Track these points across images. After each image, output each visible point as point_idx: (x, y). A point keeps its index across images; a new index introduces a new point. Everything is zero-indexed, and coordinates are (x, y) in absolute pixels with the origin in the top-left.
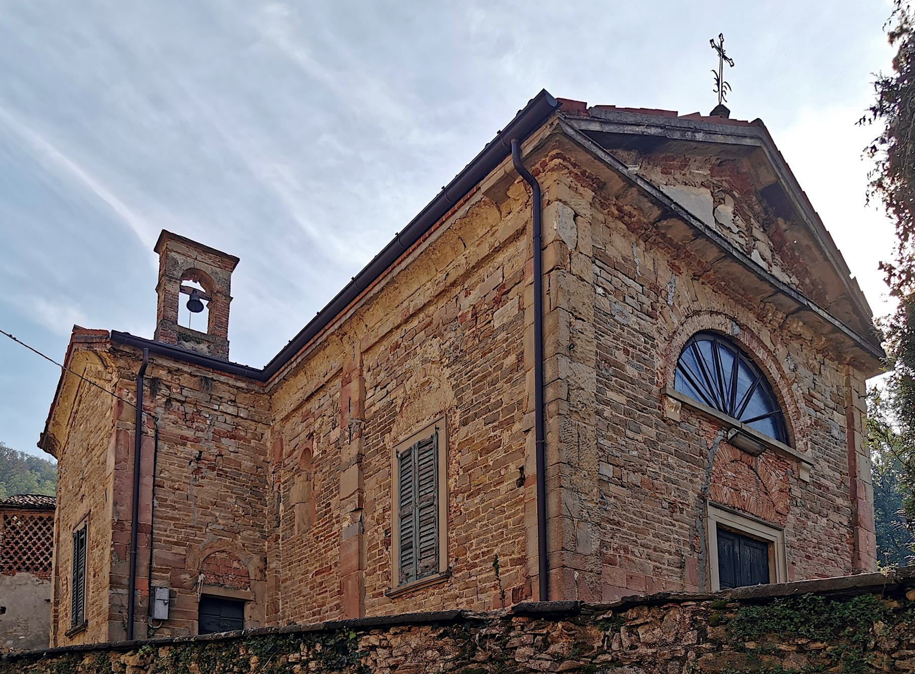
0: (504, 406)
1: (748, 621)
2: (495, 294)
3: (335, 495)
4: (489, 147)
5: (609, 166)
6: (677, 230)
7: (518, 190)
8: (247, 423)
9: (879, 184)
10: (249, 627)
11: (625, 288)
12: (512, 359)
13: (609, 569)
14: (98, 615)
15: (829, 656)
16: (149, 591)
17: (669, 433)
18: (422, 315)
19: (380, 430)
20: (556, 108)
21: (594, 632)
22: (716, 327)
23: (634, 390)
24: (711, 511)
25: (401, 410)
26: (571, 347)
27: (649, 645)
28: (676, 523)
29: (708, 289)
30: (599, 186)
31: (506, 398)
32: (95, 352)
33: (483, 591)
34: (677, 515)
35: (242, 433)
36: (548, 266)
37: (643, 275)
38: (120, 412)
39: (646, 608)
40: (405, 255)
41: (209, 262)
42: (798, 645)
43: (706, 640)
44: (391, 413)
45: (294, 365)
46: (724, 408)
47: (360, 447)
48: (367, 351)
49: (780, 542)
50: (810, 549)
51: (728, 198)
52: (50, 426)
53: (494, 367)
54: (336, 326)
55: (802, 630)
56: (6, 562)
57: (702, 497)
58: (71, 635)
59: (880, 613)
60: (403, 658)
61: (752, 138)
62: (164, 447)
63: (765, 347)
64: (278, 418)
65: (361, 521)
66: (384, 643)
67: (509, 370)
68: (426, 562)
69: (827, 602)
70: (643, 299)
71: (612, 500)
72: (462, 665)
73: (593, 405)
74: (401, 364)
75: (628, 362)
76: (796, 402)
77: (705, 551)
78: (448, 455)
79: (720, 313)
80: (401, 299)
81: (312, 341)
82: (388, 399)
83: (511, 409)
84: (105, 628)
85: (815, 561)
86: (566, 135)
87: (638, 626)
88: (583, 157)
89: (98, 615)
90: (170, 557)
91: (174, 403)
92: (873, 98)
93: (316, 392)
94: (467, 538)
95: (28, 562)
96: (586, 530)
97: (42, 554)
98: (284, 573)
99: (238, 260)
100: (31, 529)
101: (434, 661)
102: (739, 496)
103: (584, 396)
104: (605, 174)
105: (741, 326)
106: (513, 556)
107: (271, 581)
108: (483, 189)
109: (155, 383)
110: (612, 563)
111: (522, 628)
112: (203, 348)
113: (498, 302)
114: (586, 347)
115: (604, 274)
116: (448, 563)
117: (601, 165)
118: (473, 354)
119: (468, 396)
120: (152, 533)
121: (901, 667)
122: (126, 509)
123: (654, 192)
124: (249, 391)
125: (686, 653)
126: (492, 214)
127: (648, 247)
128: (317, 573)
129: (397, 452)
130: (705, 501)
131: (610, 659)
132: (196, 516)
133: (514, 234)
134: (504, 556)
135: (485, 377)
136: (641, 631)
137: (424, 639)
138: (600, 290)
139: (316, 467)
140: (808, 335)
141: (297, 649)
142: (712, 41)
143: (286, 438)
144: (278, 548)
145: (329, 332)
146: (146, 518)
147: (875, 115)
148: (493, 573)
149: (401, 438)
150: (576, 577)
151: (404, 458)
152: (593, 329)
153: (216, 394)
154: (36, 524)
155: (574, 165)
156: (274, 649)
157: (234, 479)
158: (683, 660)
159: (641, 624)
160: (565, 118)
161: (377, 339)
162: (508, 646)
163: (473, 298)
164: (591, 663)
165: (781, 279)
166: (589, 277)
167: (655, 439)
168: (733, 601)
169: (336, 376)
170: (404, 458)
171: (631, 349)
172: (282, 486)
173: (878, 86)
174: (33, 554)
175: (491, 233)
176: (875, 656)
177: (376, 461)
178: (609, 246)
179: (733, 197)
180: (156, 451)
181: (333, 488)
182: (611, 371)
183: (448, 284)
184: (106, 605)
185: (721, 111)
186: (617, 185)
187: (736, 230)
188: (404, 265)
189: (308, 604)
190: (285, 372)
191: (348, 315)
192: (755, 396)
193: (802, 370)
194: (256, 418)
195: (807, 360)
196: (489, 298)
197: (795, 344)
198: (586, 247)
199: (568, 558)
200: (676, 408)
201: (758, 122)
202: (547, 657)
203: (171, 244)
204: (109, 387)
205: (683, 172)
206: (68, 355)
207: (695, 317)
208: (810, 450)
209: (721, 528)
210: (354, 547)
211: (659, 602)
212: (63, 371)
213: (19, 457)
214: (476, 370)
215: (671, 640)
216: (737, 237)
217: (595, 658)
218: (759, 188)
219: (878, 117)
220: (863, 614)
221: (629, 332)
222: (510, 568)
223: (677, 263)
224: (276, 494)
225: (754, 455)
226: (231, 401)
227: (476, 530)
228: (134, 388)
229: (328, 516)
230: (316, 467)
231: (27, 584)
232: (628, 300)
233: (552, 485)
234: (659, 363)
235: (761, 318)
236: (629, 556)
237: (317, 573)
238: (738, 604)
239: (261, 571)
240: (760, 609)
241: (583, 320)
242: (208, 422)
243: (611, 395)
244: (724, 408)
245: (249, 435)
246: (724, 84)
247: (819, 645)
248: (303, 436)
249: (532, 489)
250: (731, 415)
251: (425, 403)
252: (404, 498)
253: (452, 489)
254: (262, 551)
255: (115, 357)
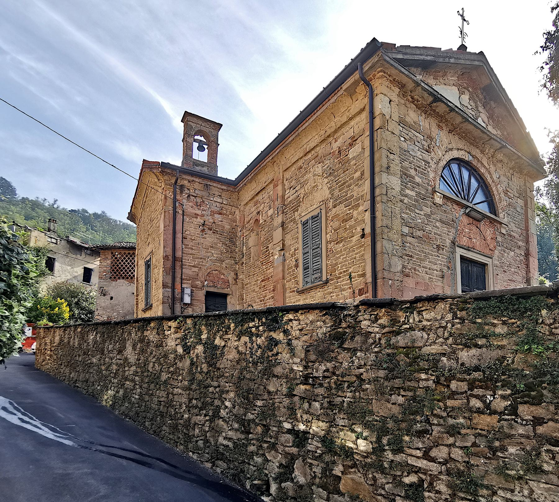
0: (354, 198)
1: (478, 309)
2: (350, 141)
3: (271, 242)
4: (347, 67)
5: (407, 76)
6: (441, 108)
7: (362, 89)
8: (227, 207)
9: (545, 86)
10: (230, 308)
11: (415, 138)
12: (358, 174)
13: (406, 279)
14: (157, 301)
15: (518, 326)
16: (181, 289)
17: (437, 210)
18: (313, 152)
19: (293, 210)
20: (381, 47)
21: (401, 313)
22: (460, 157)
23: (419, 189)
24: (458, 249)
25: (303, 200)
26: (388, 168)
27: (428, 320)
28: (440, 256)
29: (457, 137)
30: (402, 86)
31: (355, 194)
32: (153, 173)
33: (344, 290)
34: (441, 251)
35: (225, 212)
36: (376, 127)
37: (424, 131)
38: (166, 202)
39: (427, 302)
40: (304, 122)
41: (208, 126)
42: (502, 320)
43: (457, 318)
44: (298, 203)
45: (250, 177)
46: (464, 197)
47: (283, 219)
48: (286, 170)
49: (491, 264)
50: (505, 267)
51: (466, 92)
52: (133, 209)
53: (349, 178)
54: (270, 158)
55: (505, 313)
56: (113, 275)
57: (453, 243)
58: (144, 311)
59: (545, 305)
60: (306, 325)
61: (478, 61)
62: (187, 219)
63: (485, 167)
64: (242, 204)
65: (284, 255)
66: (296, 318)
67: (357, 180)
68: (316, 276)
69: (517, 299)
70: (424, 143)
71: (408, 245)
72: (335, 329)
73: (399, 197)
74: (302, 177)
75: (416, 175)
76: (500, 194)
77: (454, 269)
78: (326, 222)
79: (462, 150)
80: (302, 144)
81: (259, 166)
82: (296, 194)
83: (357, 199)
84: (161, 308)
85: (508, 273)
86: (385, 60)
87: (422, 311)
88: (394, 72)
89: (157, 301)
90: (191, 273)
91: (191, 197)
92: (542, 41)
93: (261, 191)
94: (336, 264)
95: (123, 275)
96: (395, 260)
97: (130, 271)
98: (246, 281)
99: (222, 125)
100: (124, 258)
101: (321, 327)
102: (471, 242)
103: (394, 193)
104: (405, 80)
105: (473, 156)
106: (359, 273)
107: (240, 285)
108: (344, 88)
109: (182, 187)
110: (408, 276)
111: (365, 311)
112: (205, 170)
113: (351, 145)
114: (396, 167)
115: (404, 130)
116: (327, 276)
117: (403, 76)
118: (339, 171)
119: (336, 193)
120: (182, 261)
121: (555, 333)
122: (169, 250)
123: (429, 89)
124: (228, 191)
125: (447, 324)
126: (348, 101)
127: (427, 116)
128: (262, 281)
129: (301, 221)
130: (455, 244)
131: (408, 327)
132: (203, 253)
133: (359, 111)
134: (354, 273)
135: (345, 183)
136: (424, 313)
137: (316, 316)
138: (402, 139)
139: (261, 228)
140: (505, 160)
141: (253, 321)
142: (458, 12)
143: (246, 213)
144: (243, 268)
145: (267, 161)
146: (179, 254)
147: (543, 50)
148: (349, 281)
149: (303, 214)
150: (390, 283)
151: (305, 224)
152: (399, 159)
153: (211, 192)
154: (127, 256)
155: (390, 76)
156: (242, 320)
157: (221, 235)
158: (445, 328)
159: (424, 310)
160: (385, 52)
161: (291, 164)
162: (357, 320)
163: (338, 144)
164: (399, 329)
165: (493, 133)
166: (397, 132)
167: (430, 213)
168: (470, 298)
169: (271, 183)
170: (305, 224)
171: (418, 168)
172: (245, 238)
173: (545, 35)
174: (126, 271)
175: (347, 110)
176: (542, 327)
177: (291, 225)
178: (407, 117)
179: (469, 91)
180: (183, 221)
181: (269, 239)
182: (408, 180)
183: (326, 136)
184: (161, 296)
185: (463, 47)
186: (411, 85)
187: (470, 107)
188: (304, 127)
189: (258, 296)
190: (246, 181)
191: (276, 152)
192: (480, 191)
193: (502, 178)
194: (232, 204)
195: (505, 173)
196: (347, 143)
197: (499, 165)
198: (396, 117)
199: (386, 274)
200: (440, 198)
201: (481, 53)
202: (377, 326)
203: (189, 118)
204: (160, 190)
205: (444, 78)
206: (141, 174)
207: (450, 152)
208: (506, 218)
209: (462, 257)
210: (281, 268)
211: (434, 299)
212: (138, 182)
213: (118, 223)
214: (340, 180)
215: (439, 318)
216: (470, 111)
217: (401, 326)
218: (482, 86)
219: (545, 51)
220: (536, 306)
221: (417, 160)
222: (357, 279)
223: (441, 124)
224: (242, 242)
225: (479, 221)
226: (219, 196)
227: (341, 260)
228: (172, 190)
229: (267, 253)
230: (261, 228)
231: (123, 285)
232: (416, 143)
233: (378, 238)
234: (432, 175)
235: (482, 152)
236: (416, 272)
237: (262, 281)
238: (473, 300)
239: (235, 280)
240: (484, 303)
241: (394, 154)
242: (208, 206)
243: (408, 192)
244: (464, 197)
245: (228, 212)
246: (464, 34)
247: (513, 321)
248: (255, 213)
249: (368, 240)
250: (468, 201)
251: (315, 196)
252: (305, 244)
253: (328, 240)
254: (235, 270)
255: (163, 175)
